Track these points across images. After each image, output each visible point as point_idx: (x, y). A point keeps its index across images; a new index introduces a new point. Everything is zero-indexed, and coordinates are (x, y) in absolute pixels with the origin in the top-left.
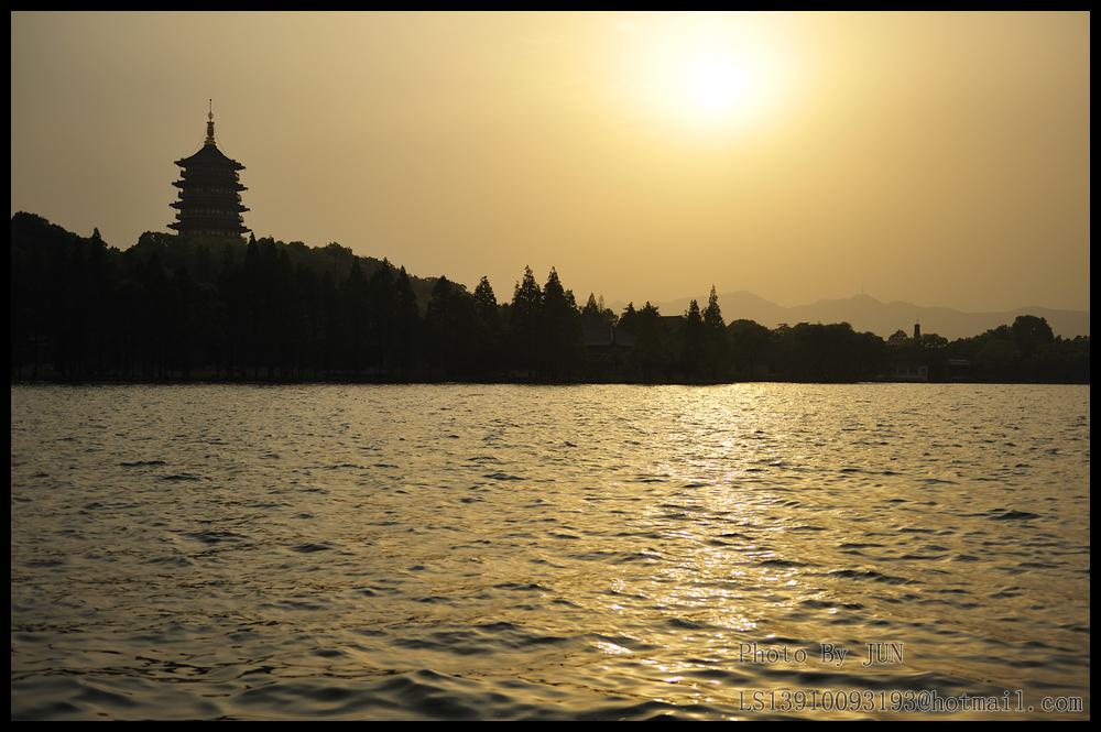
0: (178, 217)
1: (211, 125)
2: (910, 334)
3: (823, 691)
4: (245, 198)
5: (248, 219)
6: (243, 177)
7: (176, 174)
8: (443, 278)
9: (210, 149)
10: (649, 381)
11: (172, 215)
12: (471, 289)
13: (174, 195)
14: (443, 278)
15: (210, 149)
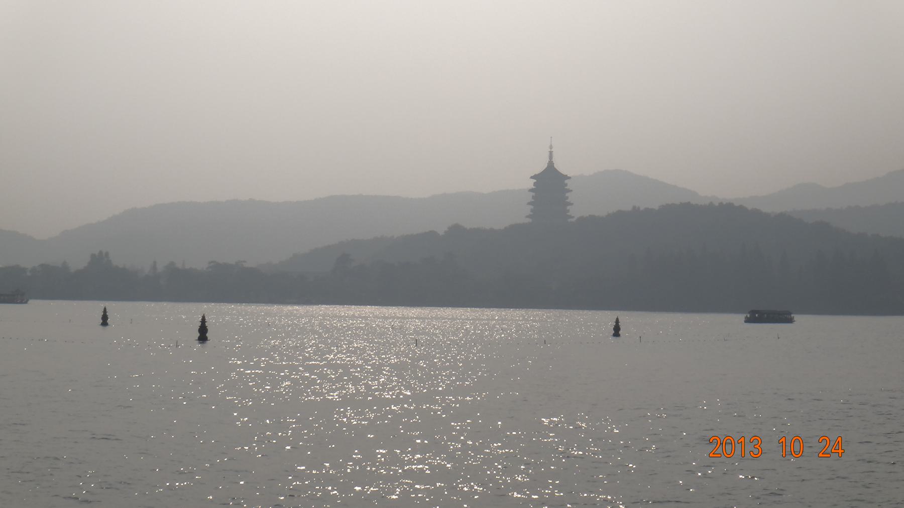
1: (551, 153)
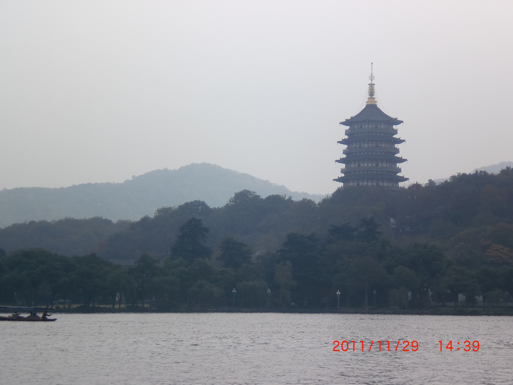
1: (372, 86)
7: (342, 132)
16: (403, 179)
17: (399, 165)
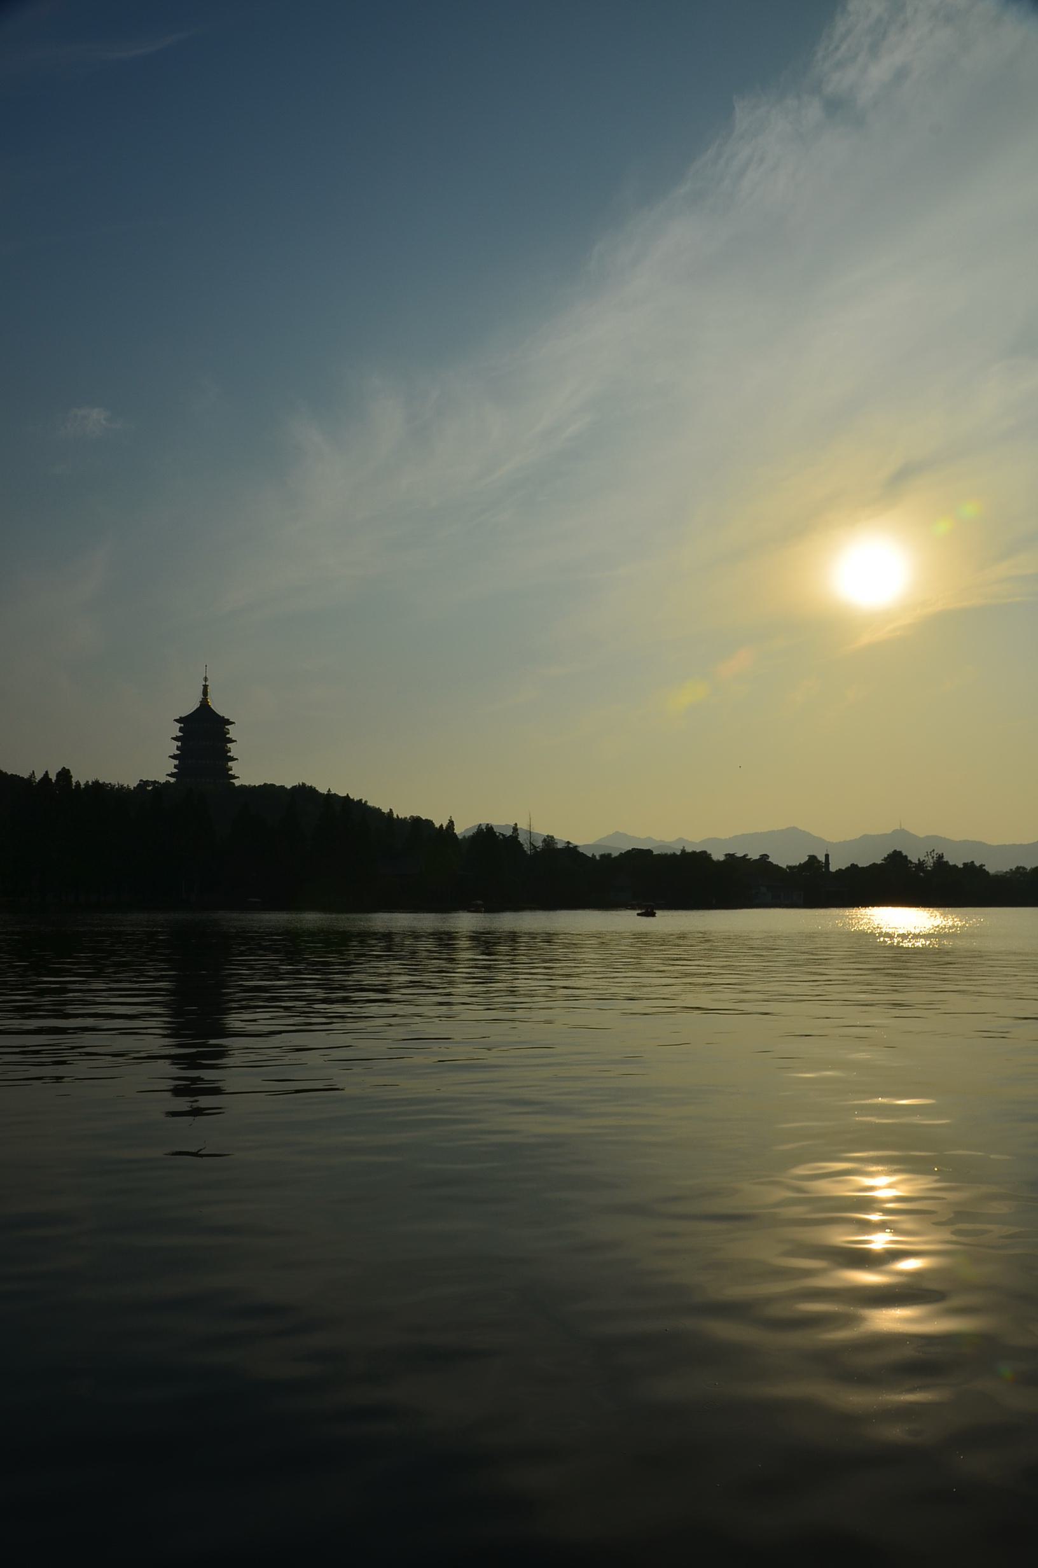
0: (175, 767)
1: (205, 687)
2: (176, 762)
3: (910, 945)
4: (234, 750)
5: (235, 768)
6: (233, 732)
7: (175, 730)
8: (764, 857)
9: (204, 708)
10: (369, 912)
11: (171, 766)
12: (679, 853)
13: (173, 748)
14: (764, 857)
15: (204, 708)
16: (234, 777)
17: (230, 764)
